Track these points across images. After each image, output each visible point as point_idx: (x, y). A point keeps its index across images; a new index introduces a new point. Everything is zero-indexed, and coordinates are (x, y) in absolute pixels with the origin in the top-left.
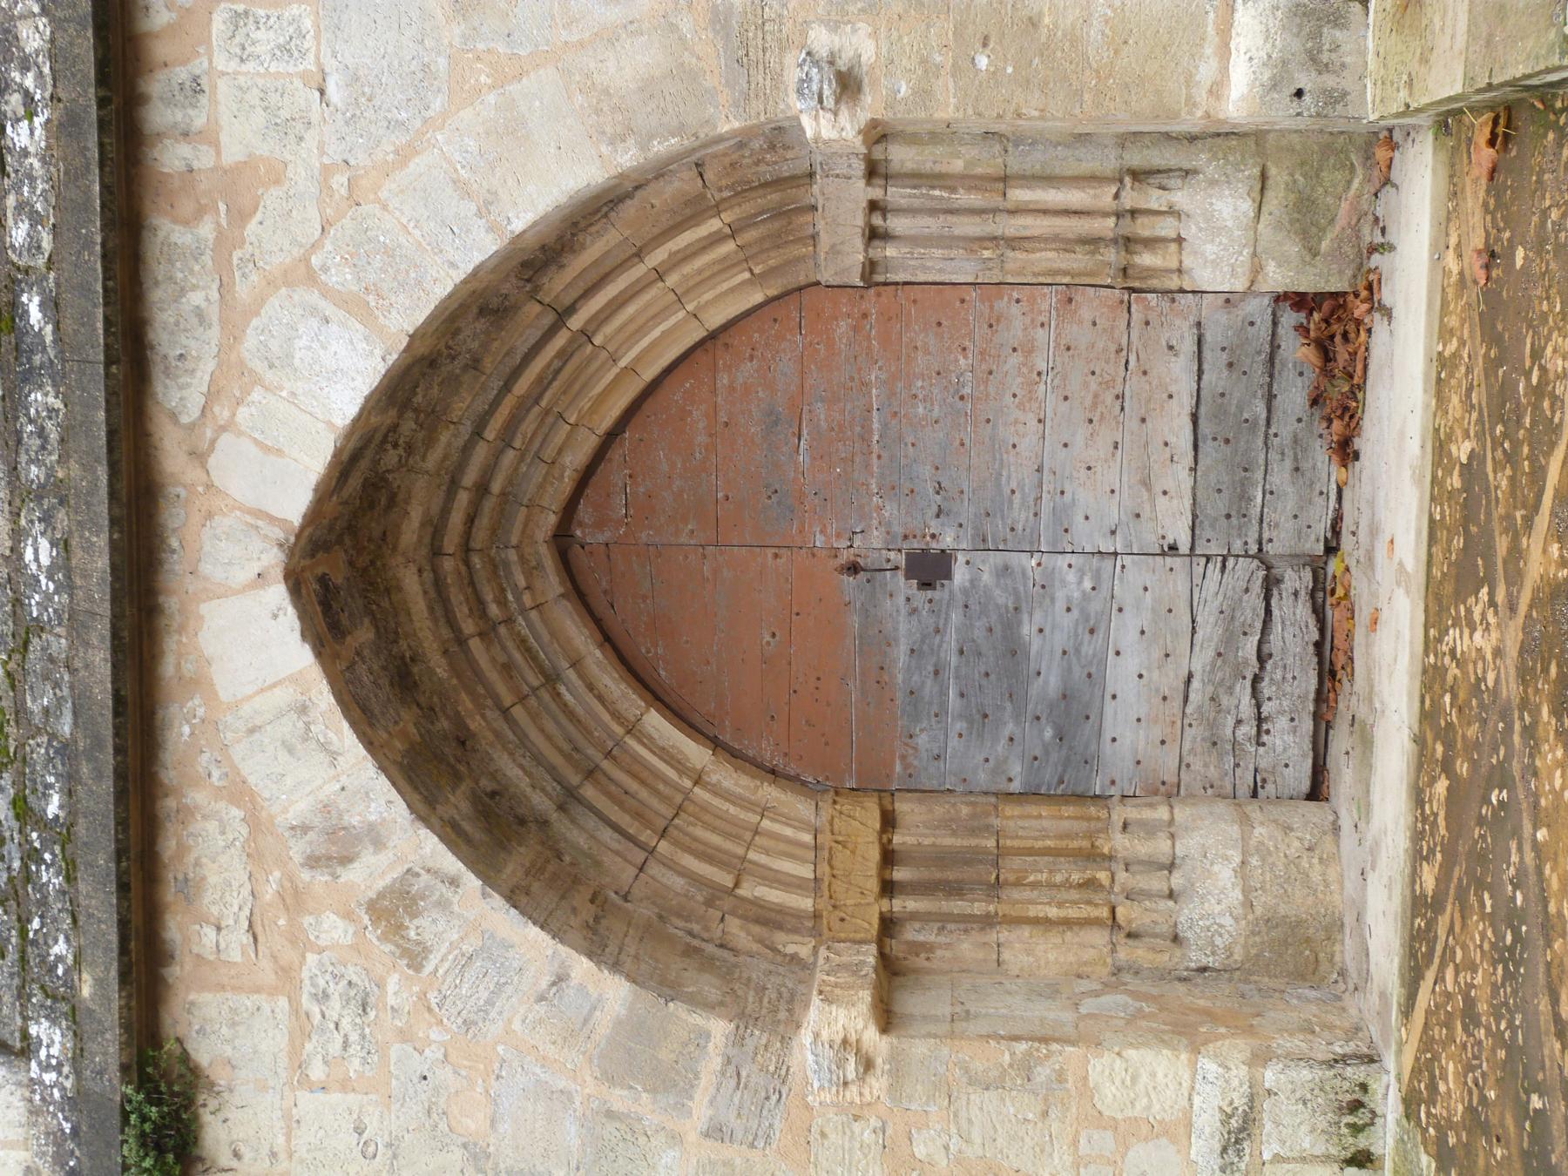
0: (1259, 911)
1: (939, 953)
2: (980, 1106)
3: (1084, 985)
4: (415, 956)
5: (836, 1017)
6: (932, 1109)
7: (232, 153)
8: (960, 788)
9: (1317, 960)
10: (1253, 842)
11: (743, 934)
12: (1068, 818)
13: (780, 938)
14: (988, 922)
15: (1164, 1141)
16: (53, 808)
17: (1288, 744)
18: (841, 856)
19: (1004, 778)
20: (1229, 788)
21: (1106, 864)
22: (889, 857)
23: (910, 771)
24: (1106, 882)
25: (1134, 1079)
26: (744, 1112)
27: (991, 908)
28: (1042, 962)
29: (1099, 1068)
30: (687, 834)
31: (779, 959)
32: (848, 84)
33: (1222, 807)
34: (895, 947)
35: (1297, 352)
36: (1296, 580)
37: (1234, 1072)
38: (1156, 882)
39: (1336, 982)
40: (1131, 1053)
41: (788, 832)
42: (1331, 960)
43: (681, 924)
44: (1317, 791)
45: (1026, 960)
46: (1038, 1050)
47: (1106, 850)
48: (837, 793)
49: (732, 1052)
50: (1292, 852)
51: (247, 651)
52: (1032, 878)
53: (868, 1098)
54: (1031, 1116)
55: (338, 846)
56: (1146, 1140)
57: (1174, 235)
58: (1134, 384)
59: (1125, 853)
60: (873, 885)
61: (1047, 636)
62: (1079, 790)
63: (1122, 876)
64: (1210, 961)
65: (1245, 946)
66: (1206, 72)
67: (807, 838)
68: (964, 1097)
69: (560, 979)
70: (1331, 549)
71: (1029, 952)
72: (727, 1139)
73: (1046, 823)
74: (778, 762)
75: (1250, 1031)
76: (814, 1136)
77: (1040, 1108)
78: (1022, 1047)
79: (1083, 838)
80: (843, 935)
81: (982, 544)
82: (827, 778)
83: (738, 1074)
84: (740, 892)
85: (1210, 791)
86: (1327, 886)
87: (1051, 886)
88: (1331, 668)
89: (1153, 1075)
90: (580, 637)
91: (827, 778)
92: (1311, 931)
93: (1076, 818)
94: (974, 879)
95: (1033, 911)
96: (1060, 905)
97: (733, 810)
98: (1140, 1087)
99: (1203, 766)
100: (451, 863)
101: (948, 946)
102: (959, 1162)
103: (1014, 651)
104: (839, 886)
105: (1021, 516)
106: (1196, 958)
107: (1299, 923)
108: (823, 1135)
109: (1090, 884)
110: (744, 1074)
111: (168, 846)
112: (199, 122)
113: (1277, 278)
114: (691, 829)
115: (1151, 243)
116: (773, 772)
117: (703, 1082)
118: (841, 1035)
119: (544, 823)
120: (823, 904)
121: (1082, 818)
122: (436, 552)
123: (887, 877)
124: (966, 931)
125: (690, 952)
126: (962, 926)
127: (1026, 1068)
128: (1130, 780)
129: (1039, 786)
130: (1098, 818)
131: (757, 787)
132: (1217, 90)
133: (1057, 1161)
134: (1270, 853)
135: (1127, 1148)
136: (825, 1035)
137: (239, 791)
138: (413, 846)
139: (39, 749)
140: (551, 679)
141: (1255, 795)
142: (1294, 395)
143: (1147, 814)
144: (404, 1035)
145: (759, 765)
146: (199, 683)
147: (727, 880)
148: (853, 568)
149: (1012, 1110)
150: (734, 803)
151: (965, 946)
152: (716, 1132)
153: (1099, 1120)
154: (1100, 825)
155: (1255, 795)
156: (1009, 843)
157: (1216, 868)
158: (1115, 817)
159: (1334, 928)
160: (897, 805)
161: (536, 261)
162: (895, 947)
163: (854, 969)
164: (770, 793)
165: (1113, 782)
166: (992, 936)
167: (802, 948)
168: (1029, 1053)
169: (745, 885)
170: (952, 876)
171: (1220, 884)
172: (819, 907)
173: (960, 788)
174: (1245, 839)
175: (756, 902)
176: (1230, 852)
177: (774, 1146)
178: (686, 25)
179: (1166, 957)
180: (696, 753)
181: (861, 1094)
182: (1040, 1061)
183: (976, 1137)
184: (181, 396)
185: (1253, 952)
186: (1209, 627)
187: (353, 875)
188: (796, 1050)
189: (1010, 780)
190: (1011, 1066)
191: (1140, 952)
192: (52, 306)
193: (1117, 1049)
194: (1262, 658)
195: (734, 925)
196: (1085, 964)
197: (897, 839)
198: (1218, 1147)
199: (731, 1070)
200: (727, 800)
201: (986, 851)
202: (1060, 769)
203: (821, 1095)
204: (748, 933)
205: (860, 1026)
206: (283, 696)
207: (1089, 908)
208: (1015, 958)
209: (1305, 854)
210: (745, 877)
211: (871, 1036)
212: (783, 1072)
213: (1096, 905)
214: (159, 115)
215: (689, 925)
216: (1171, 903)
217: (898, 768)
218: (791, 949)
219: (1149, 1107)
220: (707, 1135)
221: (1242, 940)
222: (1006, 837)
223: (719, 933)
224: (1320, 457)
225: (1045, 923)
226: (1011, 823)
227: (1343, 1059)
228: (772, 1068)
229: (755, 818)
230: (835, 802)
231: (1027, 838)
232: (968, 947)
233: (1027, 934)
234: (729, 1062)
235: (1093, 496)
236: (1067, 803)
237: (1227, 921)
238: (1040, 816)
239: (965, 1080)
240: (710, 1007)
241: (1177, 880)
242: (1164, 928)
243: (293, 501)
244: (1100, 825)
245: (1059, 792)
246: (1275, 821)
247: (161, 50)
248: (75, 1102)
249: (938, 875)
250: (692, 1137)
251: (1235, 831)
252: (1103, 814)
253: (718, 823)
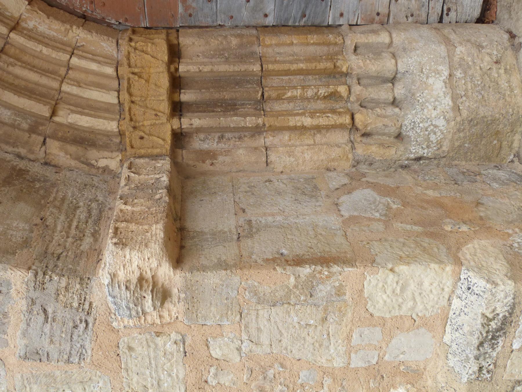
0: (465, 113)
1: (221, 159)
2: (267, 322)
5: (131, 259)
6: (225, 323)
8: (228, 24)
9: (501, 147)
10: (456, 59)
11: (62, 154)
12: (313, 44)
13: (93, 154)
14: (257, 131)
15: (423, 330)
18: (138, 85)
19: (262, 15)
20: (424, 15)
21: (343, 79)
22: (177, 83)
23: (190, 11)
24: (344, 94)
25: (403, 289)
26: (56, 339)
27: (260, 121)
28: (301, 161)
29: (374, 282)
30: (9, 73)
31: (94, 171)
33: (425, 31)
37: (502, 287)
38: (383, 93)
39: (512, 161)
40: (403, 269)
41: (94, 66)
42: (510, 147)
43: (10, 149)
45: (288, 160)
46: (320, 273)
47: (344, 69)
48: (134, 32)
49: (33, 294)
50: (485, 65)
52: (289, 94)
53: (167, 319)
54: (312, 322)
56: (408, 330)
57: (137, 51)
59: (359, 71)
60: (165, 107)
62: (317, 22)
63: (357, 89)
64: (425, 152)
65: (452, 141)
67: (110, 70)
68: (253, 313)
71: (295, 156)
72: (44, 359)
73: (296, 49)
74: (87, 8)
76: (123, 349)
77: (320, 315)
78: (306, 271)
79: (327, 60)
80: (143, 151)
82: (126, 20)
83: (45, 311)
84: (56, 119)
85: (410, 19)
86: (512, 91)
87: (303, 99)
89: (420, 284)
91: (126, 20)
92: (501, 126)
93: (318, 44)
94: (242, 96)
95: (293, 121)
96: (312, 114)
97: (45, 51)
98: (408, 293)
101: (227, 152)
102: (250, 358)
104: (137, 110)
106: (415, 150)
107: (493, 121)
108: (130, 349)
109: (334, 96)
110: (50, 310)
114: (11, 68)
116: (84, 17)
117: (13, 319)
118: (137, 274)
120: (126, 125)
121: (324, 44)
123: (176, 99)
124: (240, 138)
126: (237, 135)
127: (309, 288)
128: (354, 13)
129: (287, 20)
130: (336, 44)
131: (67, 31)
133: (332, 351)
134: (469, 67)
135: (392, 338)
136: (121, 275)
141: (441, 21)
143: (372, 39)
145: (72, 13)
147: (44, 111)
149: (296, 319)
150: (47, 45)
151: (241, 151)
153: (371, 320)
154: (337, 49)
155: (441, 21)
156: (271, 67)
157: (431, 81)
158: (348, 42)
160: (181, 39)
162: (186, 156)
164: (79, 34)
165: (342, 15)
166: (260, 141)
167: (111, 161)
168: (312, 276)
169: (61, 113)
171: (435, 93)
172: (123, 128)
173: (228, 24)
174: (450, 56)
175: (71, 126)
176: (440, 68)
177: (88, 361)
179: (393, 151)
181: (160, 317)
182: (322, 281)
183: (265, 339)
185: (457, 144)
188: (95, 290)
189: (266, 16)
190: (296, 287)
191: (374, 148)
193: (390, 266)
195: (54, 147)
196: (333, 160)
197: (182, 68)
198: (476, 342)
199: (37, 308)
200: (40, 42)
201: (252, 74)
202: (303, 6)
204: (66, 153)
205: (154, 264)
207: (335, 117)
208: (279, 159)
209: (495, 67)
210: (62, 106)
211: (165, 272)
212: (87, 306)
213: (340, 113)
215: (16, 150)
216: (397, 110)
217: (181, 10)
218: (102, 163)
219: (413, 308)
220: (26, 358)
221: (450, 136)
222: (268, 62)
223: (42, 155)
225: (303, 129)
226: (270, 50)
228: (75, 304)
229: (65, 57)
230: (131, 40)
231: (284, 62)
232: (243, 154)
233: (287, 138)
234: (33, 302)
236: (310, 33)
237: (441, 123)
238: (292, 44)
239: (254, 300)
241: (399, 91)
242: (393, 130)
244: (337, 49)
245: (302, 23)
246: (468, 41)
249: (217, 96)
250: (12, 360)
251: (442, 50)
252: (339, 40)
253: (36, 62)
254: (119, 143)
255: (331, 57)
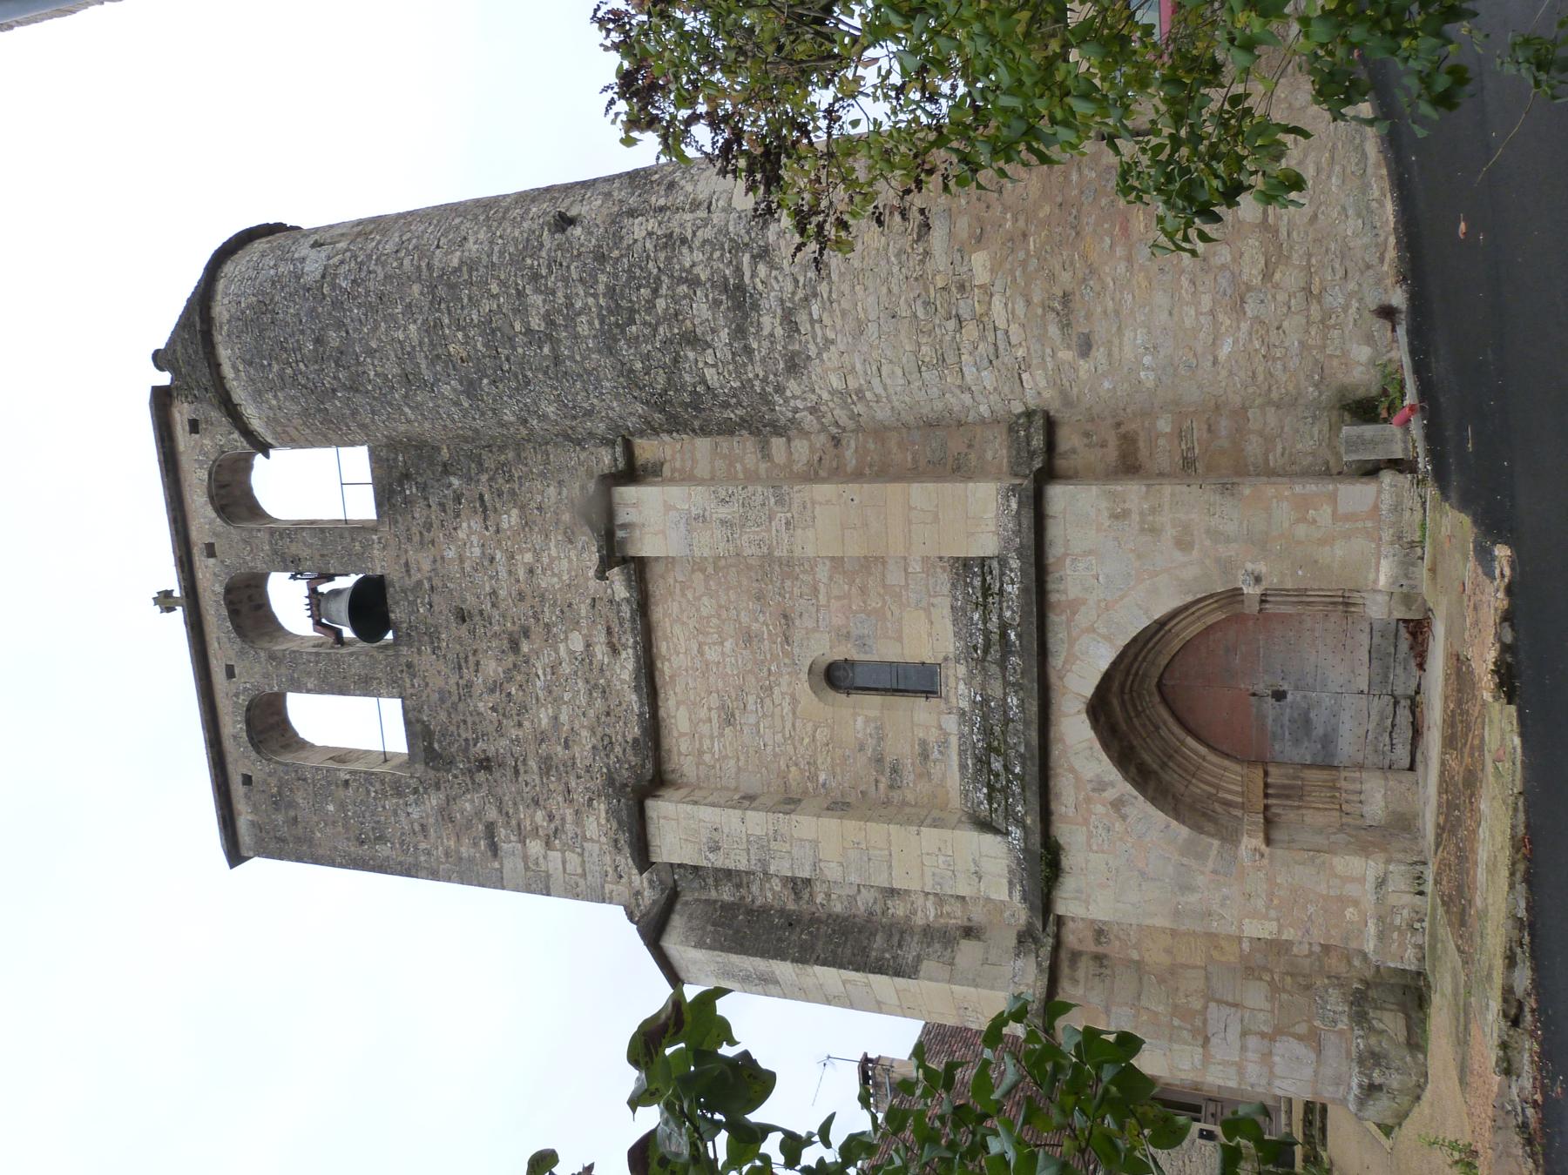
3: (1331, 830)
4: (1124, 818)
5: (1251, 842)
7: (1071, 596)
14: (1299, 807)
16: (1017, 770)
17: (1402, 754)
22: (1266, 785)
32: (1258, 580)
33: (1378, 773)
34: (1269, 814)
35: (1403, 633)
36: (1404, 703)
38: (1355, 798)
44: (1412, 768)
51: (1075, 733)
55: (1101, 786)
58: (1349, 641)
61: (1319, 719)
66: (1371, 576)
69: (1167, 826)
70: (1417, 692)
71: (1311, 818)
75: (1385, 850)
81: (1297, 688)
88: (1417, 732)
90: (1166, 715)
94: (1294, 793)
99: (1372, 759)
100: (1136, 793)
103: (1307, 721)
105: (1310, 680)
111: (1052, 784)
112: (1062, 587)
113: (1397, 615)
115: (1354, 604)
119: (1156, 773)
122: (1122, 692)
125: (1204, 814)
127: (1312, 859)
132: (1376, 581)
137: (1072, 770)
138: (1121, 786)
139: (1012, 753)
140: (1157, 728)
142: (1404, 646)
144: (1121, 839)
146: (1062, 740)
147: (1213, 791)
148: (1254, 695)
152: (1215, 872)
153: (1336, 876)
159: (1415, 816)
161: (1161, 624)
162: (1269, 814)
163: (1254, 823)
164: (1226, 763)
167: (1239, 813)
170: (1287, 793)
178: (1207, 562)
180: (1202, 750)
184: (1056, 662)
186: (1375, 718)
187: (1105, 794)
192: (1019, 636)
194: (1393, 726)
203: (1247, 863)
206: (1085, 745)
208: (1308, 820)
214: (1051, 586)
224: (1413, 664)
227: (1415, 863)
232: (1292, 815)
235: (1337, 683)
240: (1212, 836)
241: (1363, 797)
243: (1089, 691)
247: (1051, 569)
248: (1025, 850)
254: (1242, 806)
255: (1333, 781)
